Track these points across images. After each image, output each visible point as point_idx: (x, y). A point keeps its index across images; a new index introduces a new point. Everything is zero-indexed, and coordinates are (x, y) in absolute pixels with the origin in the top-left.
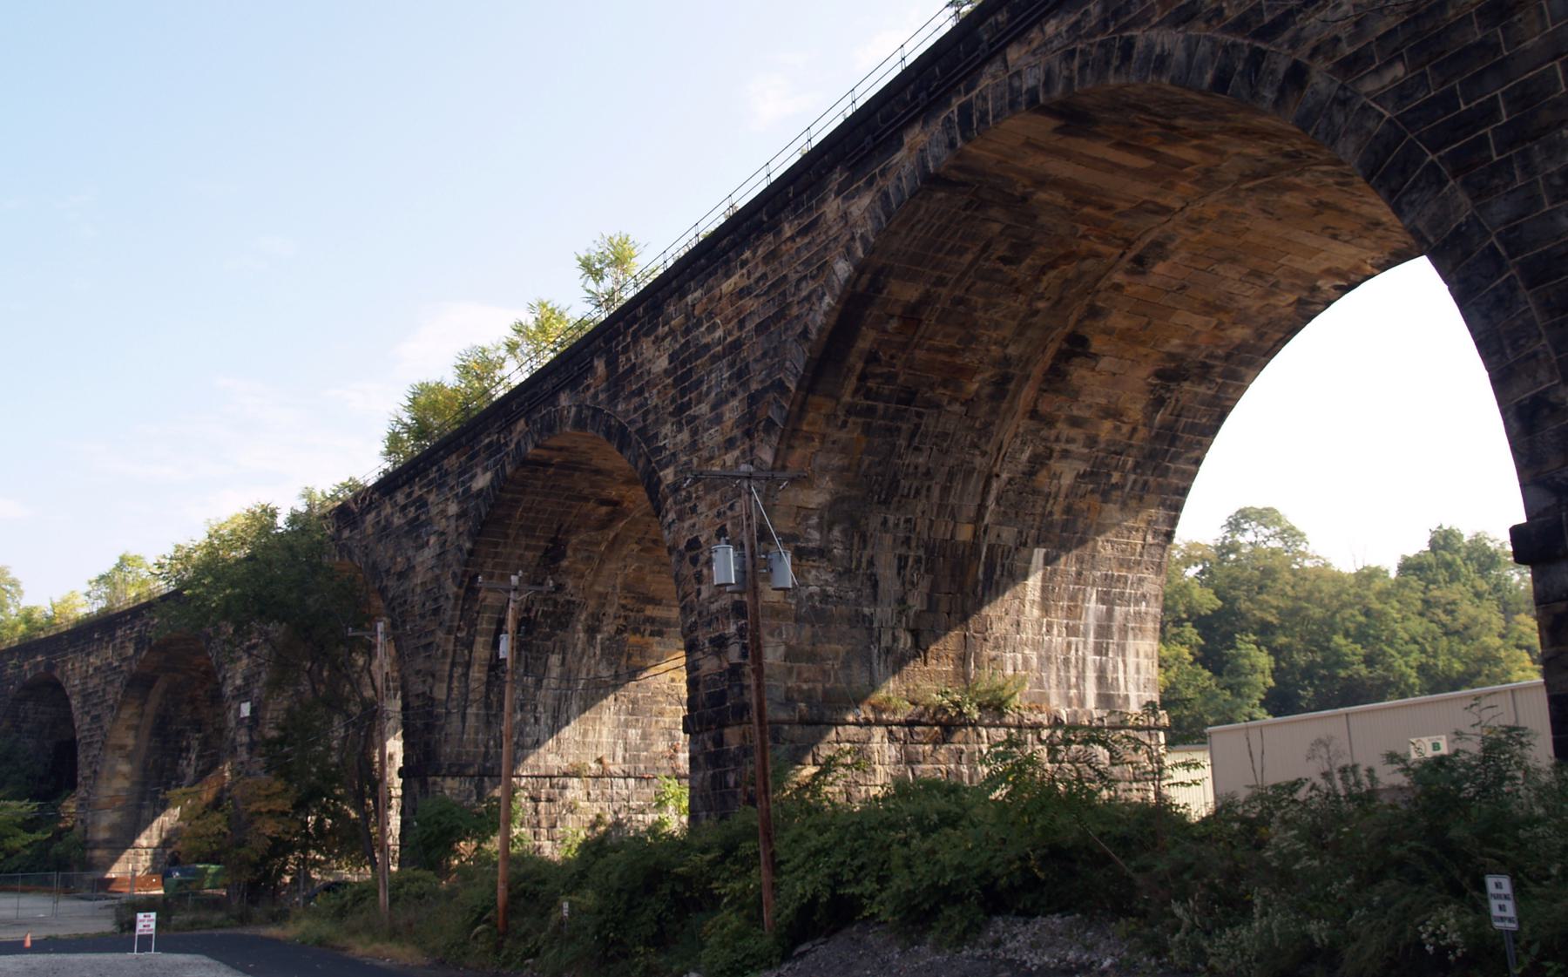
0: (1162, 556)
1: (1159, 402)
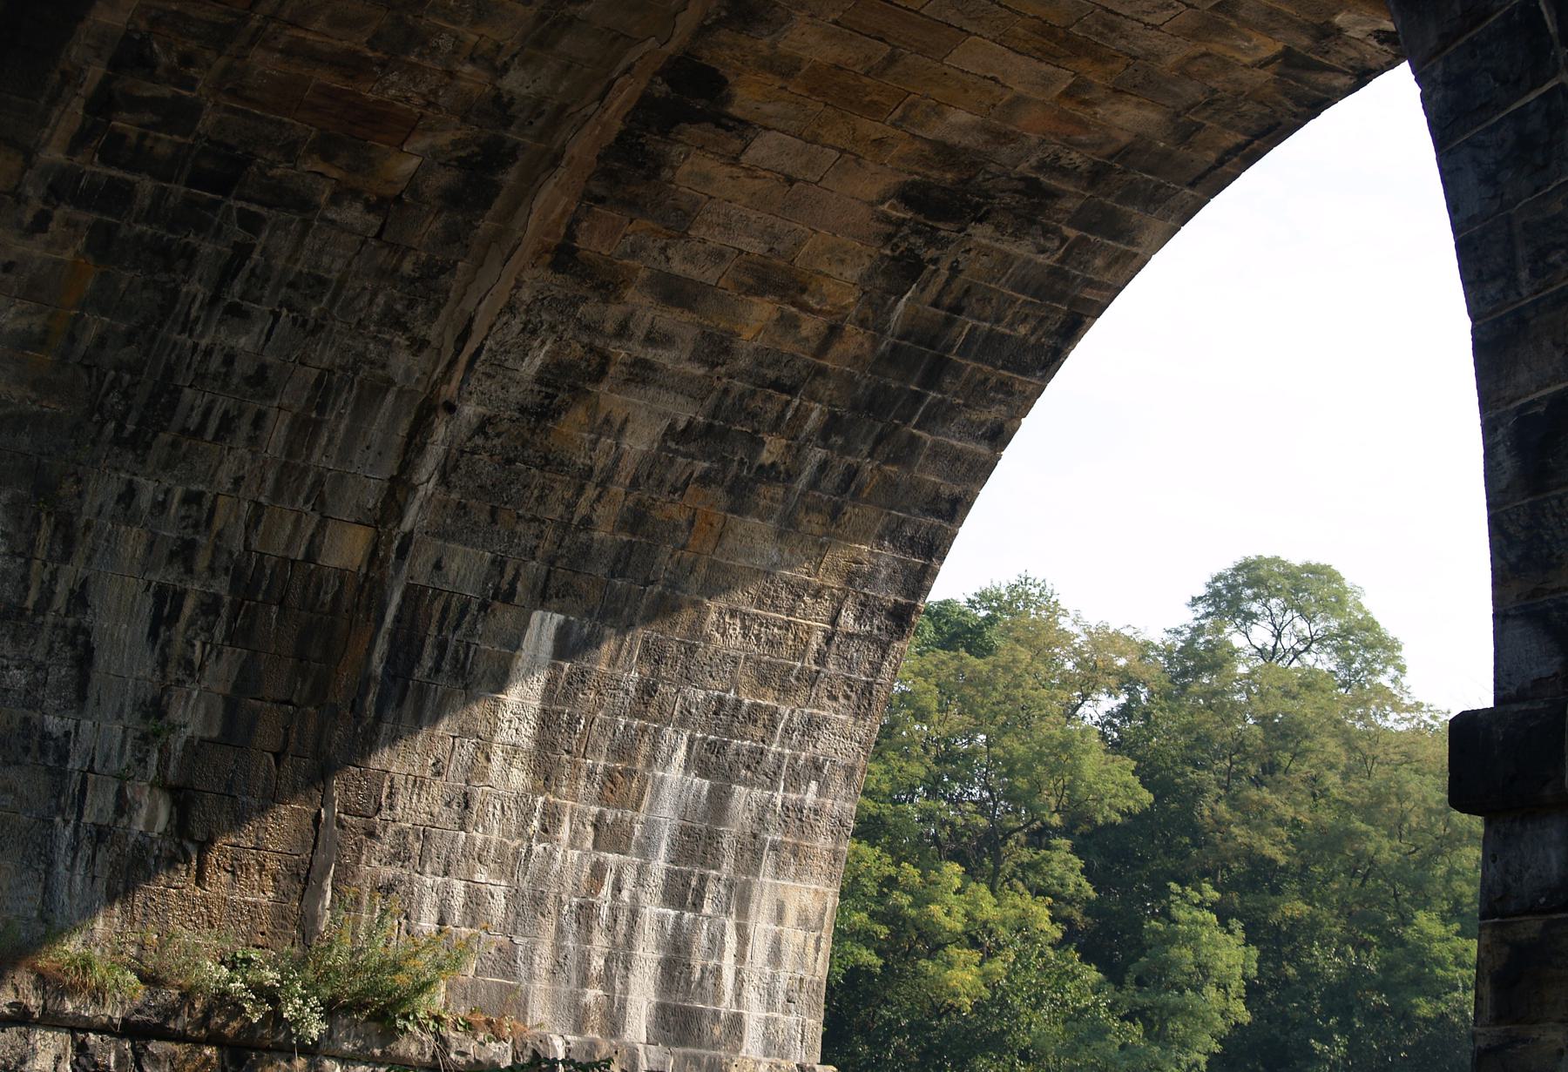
0: (876, 669)
1: (907, 269)
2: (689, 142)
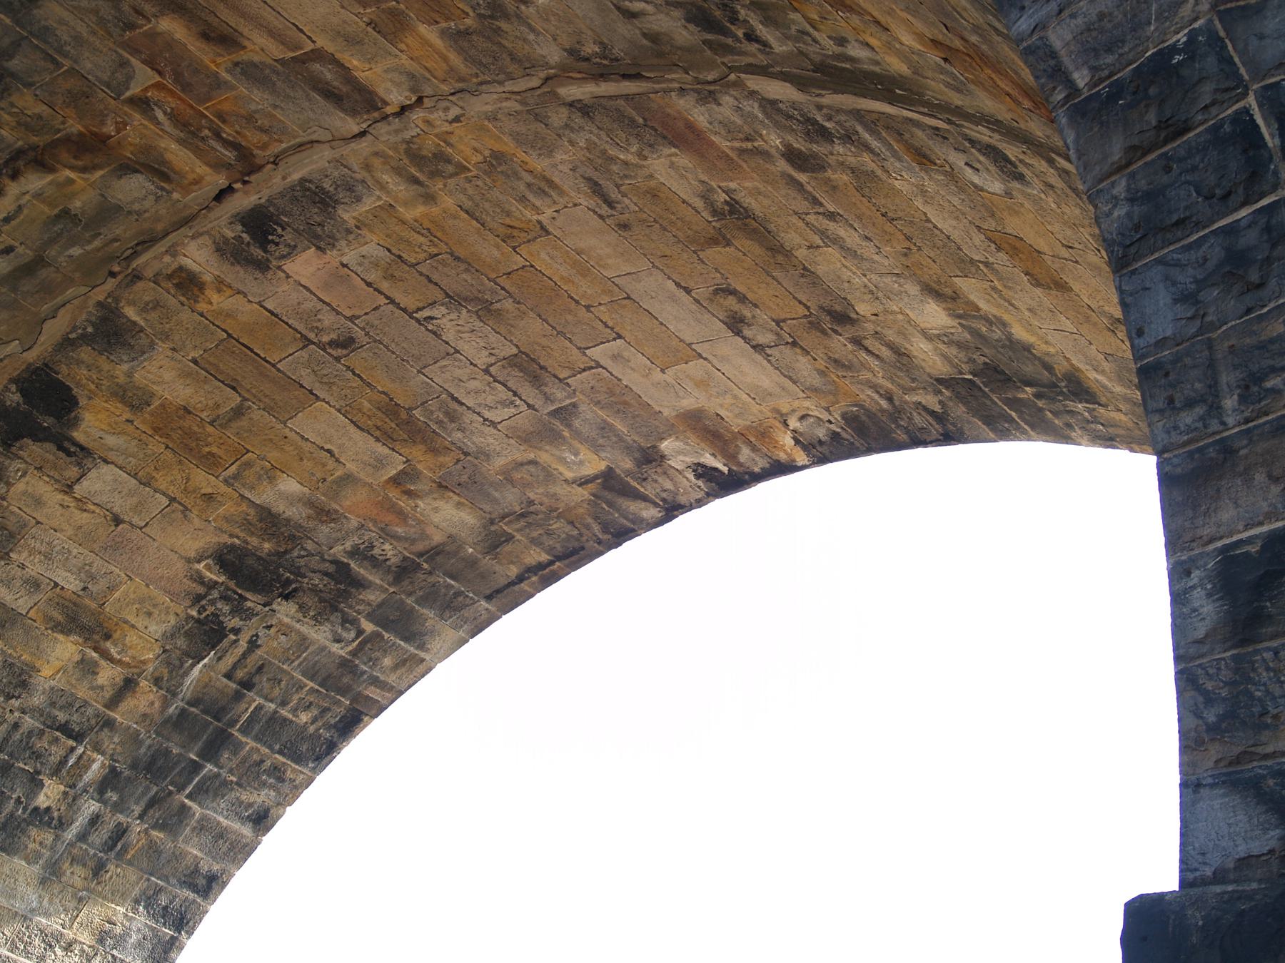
2: (28, 460)
